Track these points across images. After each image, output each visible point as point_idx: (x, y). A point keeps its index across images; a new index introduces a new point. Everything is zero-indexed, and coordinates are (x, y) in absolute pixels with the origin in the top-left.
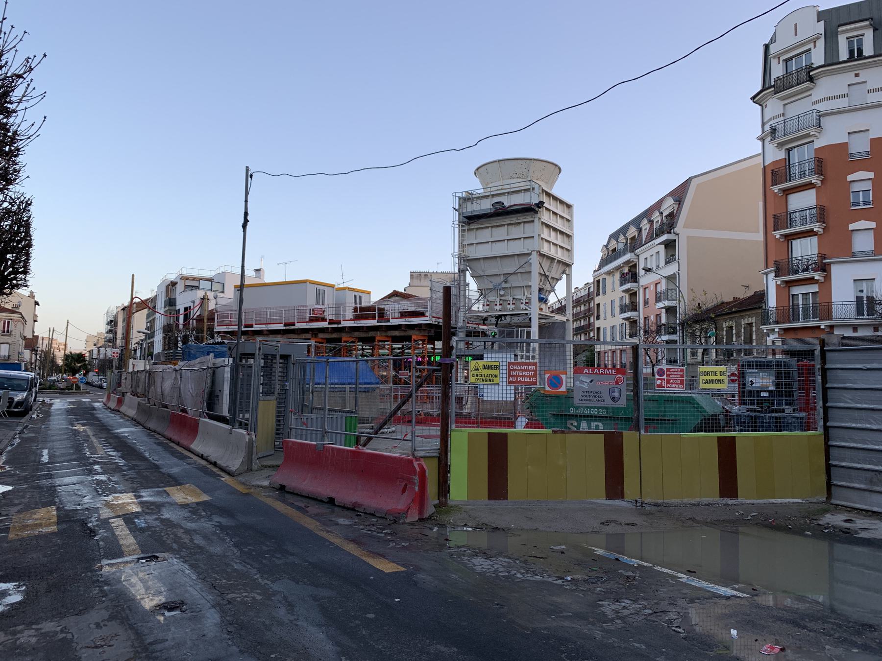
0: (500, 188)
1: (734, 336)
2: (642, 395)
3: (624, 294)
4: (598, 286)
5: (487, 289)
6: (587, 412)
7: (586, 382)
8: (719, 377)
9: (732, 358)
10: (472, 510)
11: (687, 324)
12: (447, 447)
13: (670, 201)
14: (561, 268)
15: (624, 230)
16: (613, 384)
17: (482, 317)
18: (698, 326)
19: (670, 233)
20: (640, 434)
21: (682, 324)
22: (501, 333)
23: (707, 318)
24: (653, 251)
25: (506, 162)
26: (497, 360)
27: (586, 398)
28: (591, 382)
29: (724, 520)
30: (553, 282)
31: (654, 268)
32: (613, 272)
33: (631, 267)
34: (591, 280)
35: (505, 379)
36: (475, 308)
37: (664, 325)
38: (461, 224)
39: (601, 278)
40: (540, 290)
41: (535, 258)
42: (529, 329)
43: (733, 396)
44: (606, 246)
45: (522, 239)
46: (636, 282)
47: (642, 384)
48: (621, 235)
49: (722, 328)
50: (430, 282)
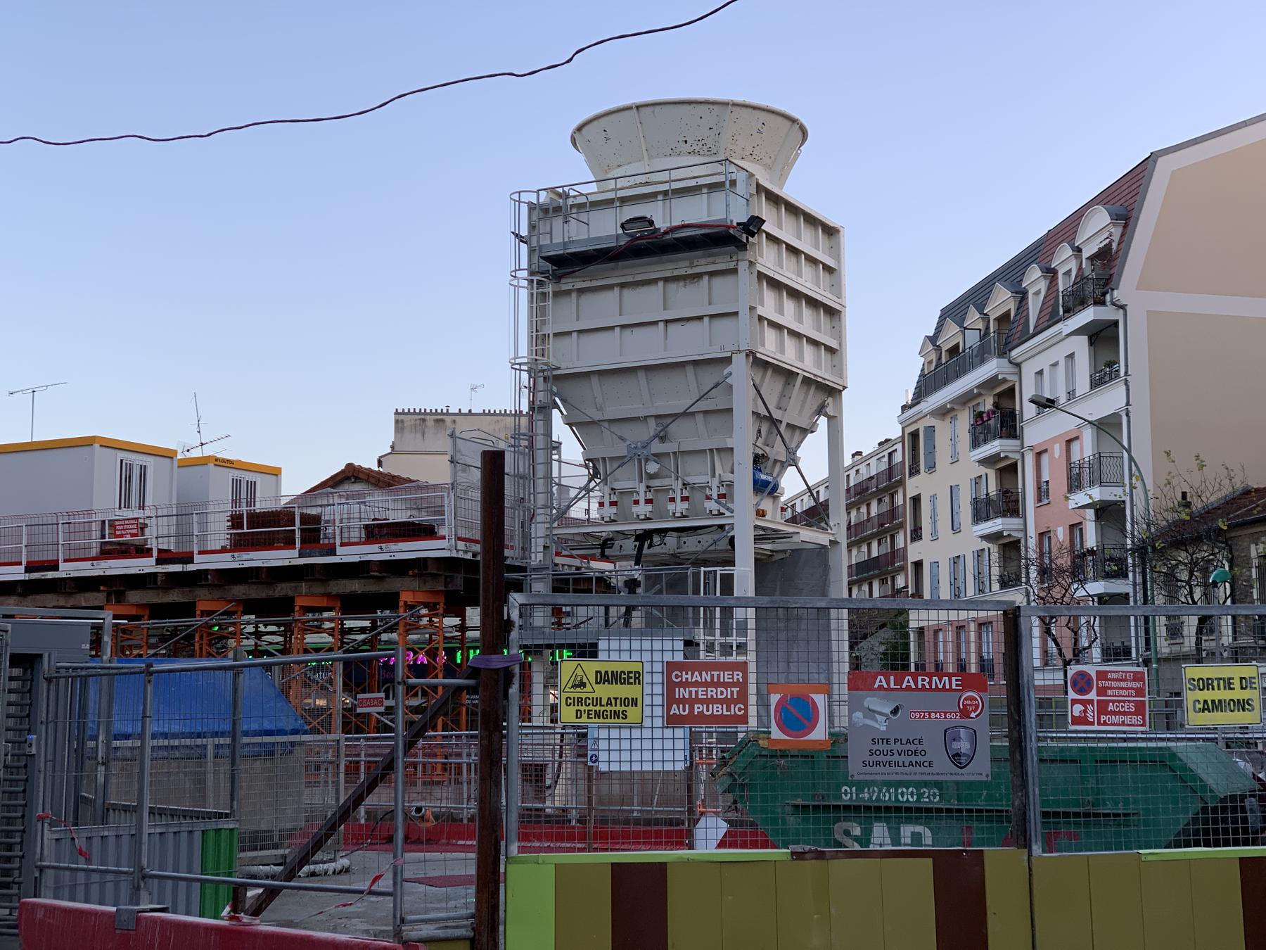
0: (643, 179)
2: (1032, 745)
3: (982, 470)
5: (612, 459)
8: (1238, 694)
12: (495, 908)
13: (1101, 219)
14: (814, 399)
15: (979, 295)
16: (954, 718)
17: (598, 538)
18: (1183, 554)
19: (1103, 303)
20: (1030, 855)
21: (1141, 550)
24: (1059, 353)
25: (658, 108)
26: (636, 656)
27: (881, 758)
28: (895, 712)
30: (792, 438)
32: (952, 409)
33: (999, 395)
34: (895, 432)
35: (658, 711)
36: (577, 512)
37: (1092, 552)
38: (535, 278)
39: (921, 426)
40: (758, 460)
41: (740, 371)
42: (727, 570)
44: (933, 339)
45: (706, 320)
46: (1015, 437)
48: (972, 308)
49: (1248, 557)
50: (449, 441)
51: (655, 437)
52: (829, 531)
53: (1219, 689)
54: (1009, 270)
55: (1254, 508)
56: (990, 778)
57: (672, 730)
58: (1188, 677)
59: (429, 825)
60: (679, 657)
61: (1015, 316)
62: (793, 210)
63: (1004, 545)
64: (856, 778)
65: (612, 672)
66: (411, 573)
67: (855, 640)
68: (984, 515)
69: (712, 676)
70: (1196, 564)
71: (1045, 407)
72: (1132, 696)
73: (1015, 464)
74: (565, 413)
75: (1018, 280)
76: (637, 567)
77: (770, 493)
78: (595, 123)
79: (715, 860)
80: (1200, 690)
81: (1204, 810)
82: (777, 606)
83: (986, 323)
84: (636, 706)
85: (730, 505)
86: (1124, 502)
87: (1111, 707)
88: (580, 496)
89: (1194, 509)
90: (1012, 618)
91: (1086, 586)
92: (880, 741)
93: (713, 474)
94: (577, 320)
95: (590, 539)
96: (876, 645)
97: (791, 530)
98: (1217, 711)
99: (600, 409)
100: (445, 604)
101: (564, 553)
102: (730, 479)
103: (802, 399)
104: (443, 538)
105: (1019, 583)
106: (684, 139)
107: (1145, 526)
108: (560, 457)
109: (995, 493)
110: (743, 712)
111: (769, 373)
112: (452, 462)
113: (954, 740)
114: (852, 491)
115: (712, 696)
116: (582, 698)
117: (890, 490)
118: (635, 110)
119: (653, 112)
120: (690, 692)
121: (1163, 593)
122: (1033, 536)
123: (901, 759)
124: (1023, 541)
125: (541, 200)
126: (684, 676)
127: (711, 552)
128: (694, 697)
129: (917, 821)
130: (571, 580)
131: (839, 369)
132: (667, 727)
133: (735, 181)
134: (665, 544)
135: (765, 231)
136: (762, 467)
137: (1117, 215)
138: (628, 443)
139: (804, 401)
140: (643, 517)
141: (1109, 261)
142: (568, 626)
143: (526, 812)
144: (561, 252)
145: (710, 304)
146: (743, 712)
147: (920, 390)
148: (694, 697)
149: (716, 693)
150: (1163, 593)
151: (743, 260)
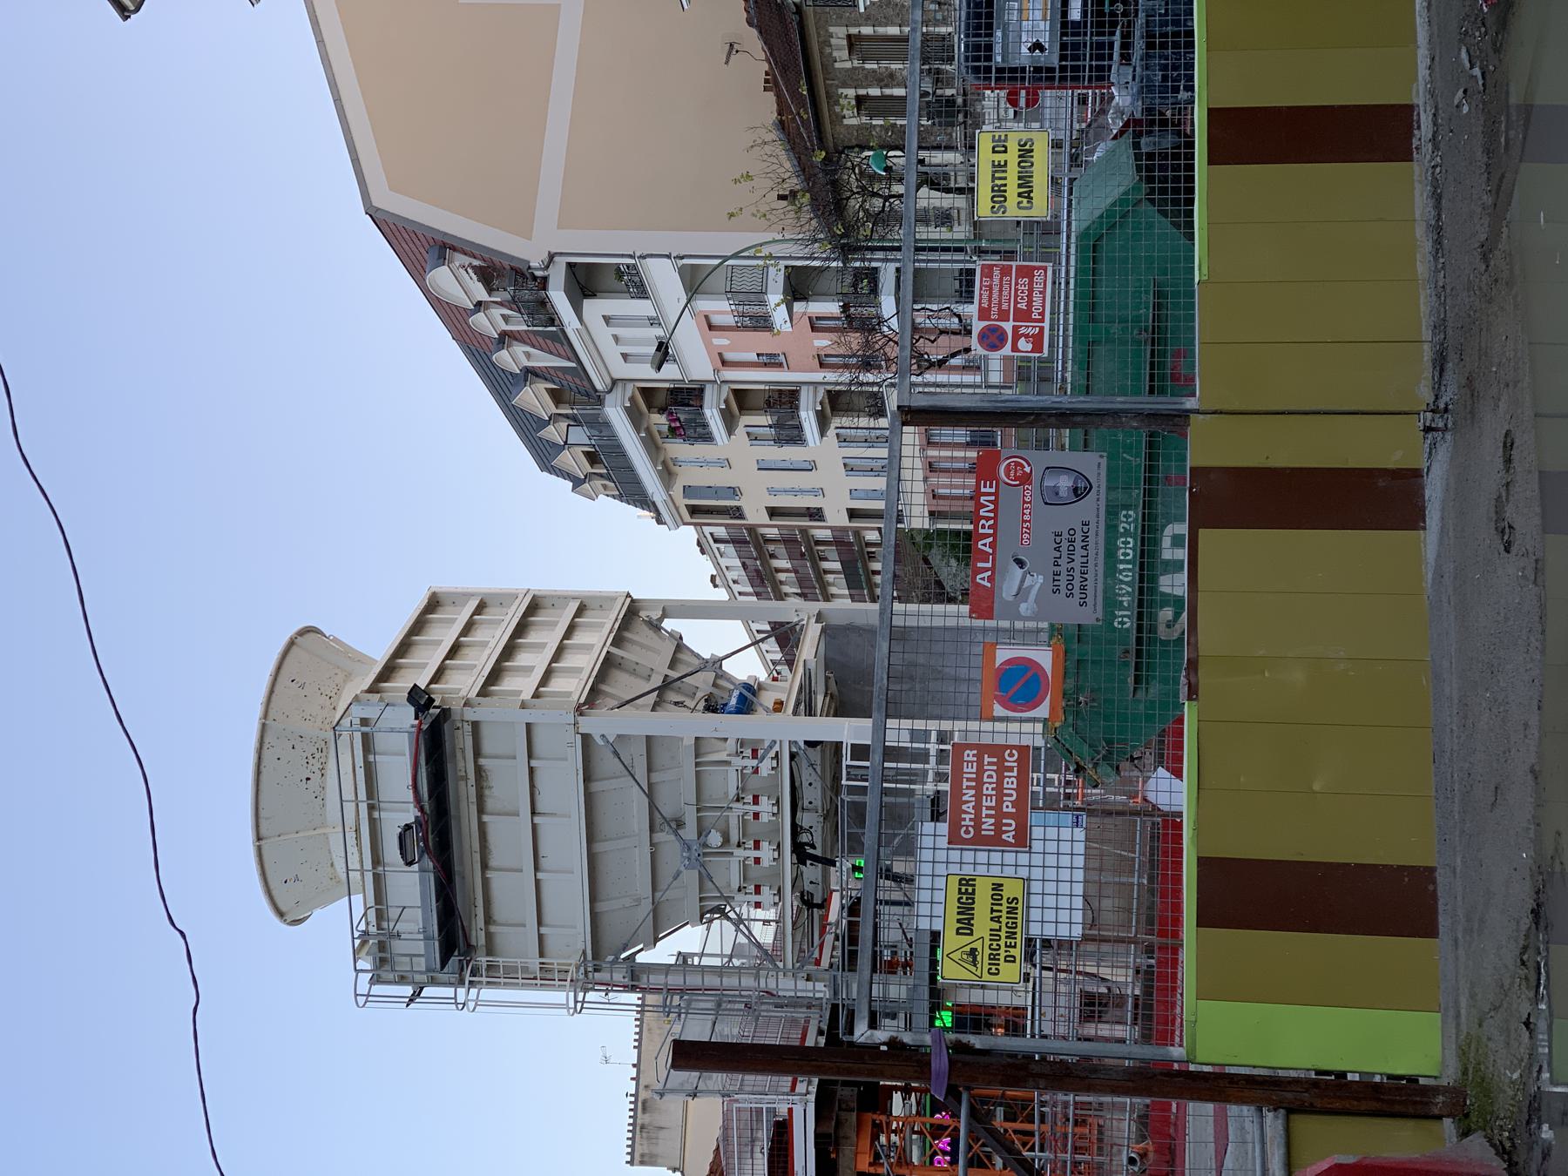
0: (351, 836)
1: (887, 92)
2: (1068, 401)
3: (740, 431)
4: (709, 511)
5: (701, 891)
6: (1127, 574)
7: (1023, 581)
8: (1012, 157)
9: (960, 100)
10: (1472, 996)
11: (843, 236)
12: (1250, 1080)
13: (443, 278)
14: (641, 634)
15: (527, 426)
16: (1031, 492)
17: (799, 910)
18: (852, 202)
19: (545, 279)
20: (1197, 412)
21: (846, 250)
22: (856, 847)
23: (826, 173)
24: (603, 334)
25: (263, 813)
26: (940, 883)
27: (1077, 583)
28: (1020, 563)
29: (1488, 151)
30: (688, 664)
31: (659, 332)
32: (664, 463)
33: (650, 407)
34: (689, 534)
35: (1010, 858)
36: (765, 935)
37: (845, 308)
38: (468, 978)
39: (682, 502)
40: (712, 707)
41: (601, 724)
42: (846, 752)
43: (1083, 101)
44: (577, 483)
45: (534, 763)
46: (702, 390)
47: (1032, 400)
48: (543, 434)
49: (860, 127)
50: (667, 1097)
51: (676, 834)
52: (804, 622)
53: (1005, 178)
54: (498, 387)
55: (801, 117)
56: (1105, 454)
57: (1033, 842)
58: (989, 214)
59: (1151, 1148)
60: (943, 828)
61: (554, 383)
62: (404, 648)
63: (833, 409)
64: (1100, 614)
65: (959, 913)
66: (833, 1156)
67: (942, 595)
68: (796, 432)
69: (968, 788)
70: (863, 188)
71: (666, 353)
72: (1011, 281)
73: (736, 392)
74: (641, 946)
75: (510, 377)
76: (838, 864)
77: (754, 694)
78: (274, 893)
79: (1196, 795)
80: (1005, 201)
81: (1152, 201)
82: (884, 703)
83: (560, 418)
84: (1002, 885)
85: (767, 744)
86: (786, 267)
87: (1023, 306)
88: (747, 932)
89: (798, 187)
90: (910, 415)
91: (886, 317)
92: (1056, 583)
93: (727, 763)
94: (524, 926)
95: (800, 922)
96: (949, 570)
97: (800, 670)
98: (1031, 182)
99: (638, 902)
100: (875, 1113)
101: (816, 955)
102: (734, 743)
103: (638, 648)
104: (790, 1110)
105: (880, 395)
106: (304, 781)
107: (817, 245)
108: (695, 954)
109: (769, 417)
110: (1014, 751)
111: (604, 687)
112: (695, 1096)
113: (1057, 494)
114: (758, 589)
115: (993, 789)
116: (990, 955)
117: (760, 544)
118: (262, 842)
119: (267, 819)
120: (987, 816)
121: (897, 228)
122: (823, 375)
123: (1078, 560)
124: (829, 388)
125: (368, 966)
126: (967, 822)
127: (823, 770)
128: (993, 812)
129: (1156, 542)
130: (851, 948)
131: (604, 601)
132: (1030, 847)
133: (362, 719)
134: (811, 827)
135: (428, 685)
136: (721, 702)
137: (439, 258)
138: (682, 868)
139: (642, 646)
140: (776, 853)
141: (494, 270)
142: (908, 954)
143: (1139, 1021)
144: (437, 944)
145: (515, 758)
146: (1014, 751)
147: (638, 501)
148: (993, 812)
149: (990, 783)
150: (897, 228)
151: (462, 715)
